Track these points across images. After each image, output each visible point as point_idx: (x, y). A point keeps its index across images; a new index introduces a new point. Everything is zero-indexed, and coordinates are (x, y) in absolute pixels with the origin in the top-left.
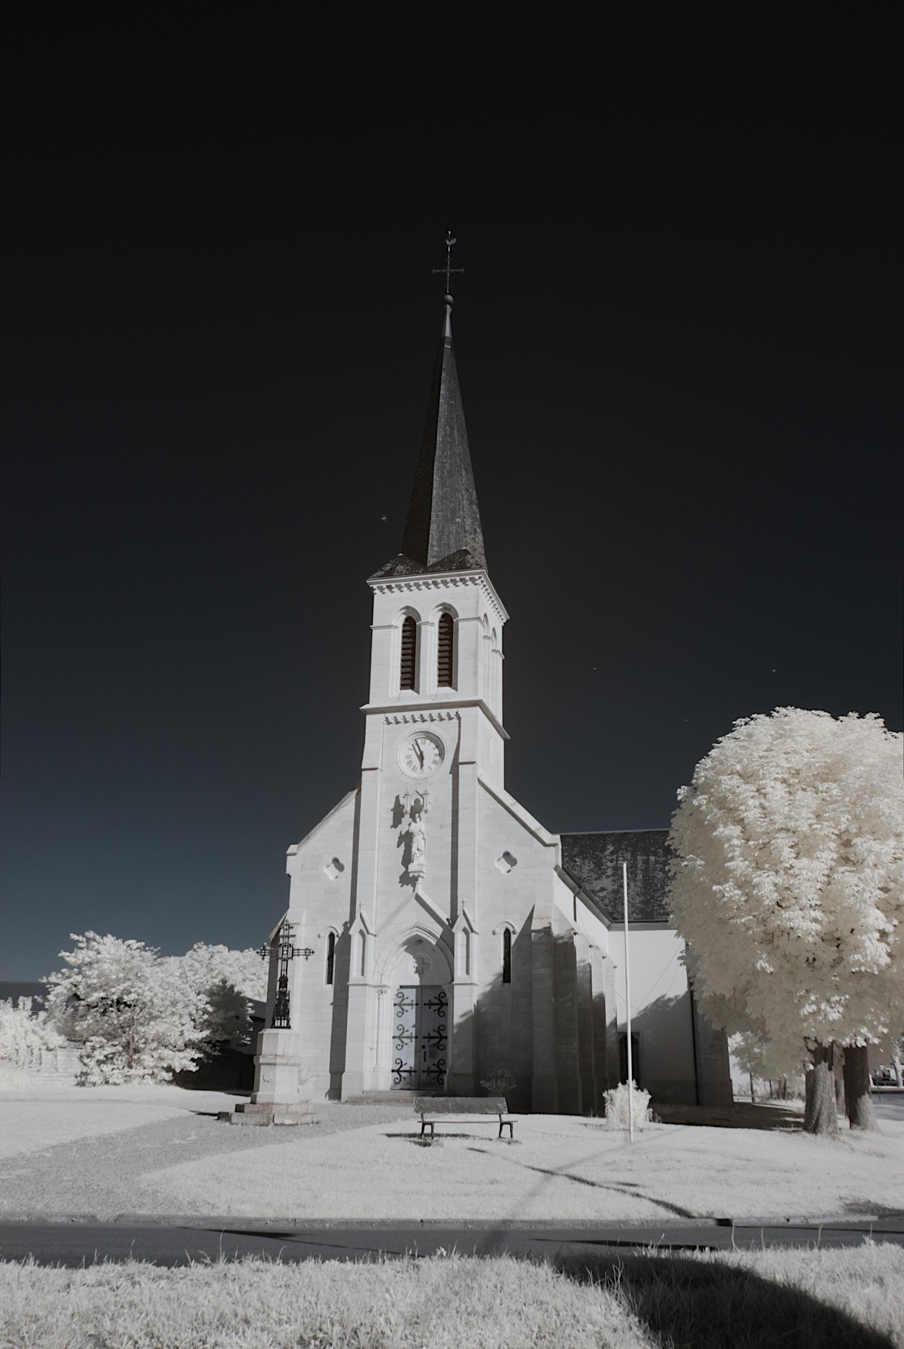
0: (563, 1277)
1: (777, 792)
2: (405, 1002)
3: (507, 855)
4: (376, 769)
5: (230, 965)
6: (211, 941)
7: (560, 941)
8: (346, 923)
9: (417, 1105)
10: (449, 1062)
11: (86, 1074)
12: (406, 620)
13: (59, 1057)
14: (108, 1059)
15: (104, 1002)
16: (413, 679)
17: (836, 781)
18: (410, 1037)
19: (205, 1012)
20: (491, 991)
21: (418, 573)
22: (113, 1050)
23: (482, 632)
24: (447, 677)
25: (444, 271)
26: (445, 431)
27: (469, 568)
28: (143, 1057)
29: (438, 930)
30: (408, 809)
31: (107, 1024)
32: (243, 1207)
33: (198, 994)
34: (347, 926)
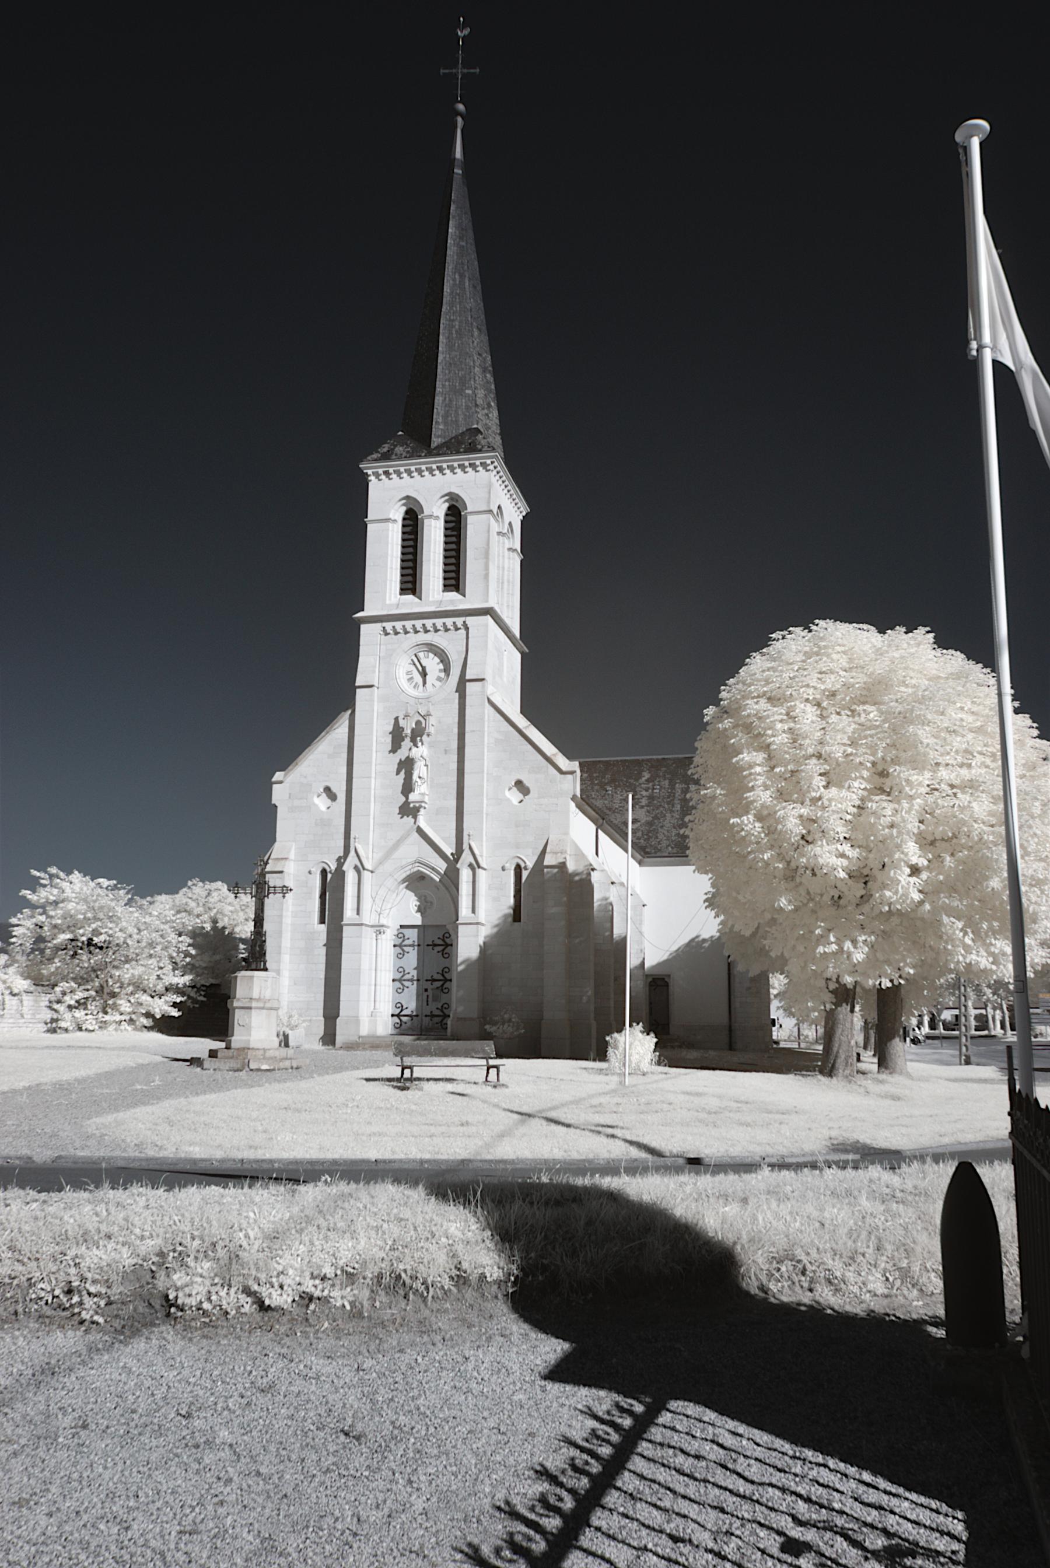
0: (433, 1199)
1: (808, 715)
2: (406, 942)
3: (519, 784)
4: (371, 686)
5: (230, 904)
6: (208, 877)
7: (577, 878)
8: (340, 857)
9: (396, 1048)
10: (453, 1006)
11: (57, 1020)
12: (407, 513)
13: (25, 1003)
14: (81, 1004)
15: (73, 943)
16: (414, 583)
17: (875, 704)
18: (411, 980)
19: (187, 954)
20: (497, 933)
21: (420, 457)
22: (86, 994)
23: (495, 527)
24: (454, 580)
25: (454, 71)
26: (454, 280)
27: (480, 451)
28: (119, 1002)
29: (442, 866)
30: (408, 731)
31: (79, 967)
32: (191, 1149)
33: (180, 935)
34: (341, 861)
